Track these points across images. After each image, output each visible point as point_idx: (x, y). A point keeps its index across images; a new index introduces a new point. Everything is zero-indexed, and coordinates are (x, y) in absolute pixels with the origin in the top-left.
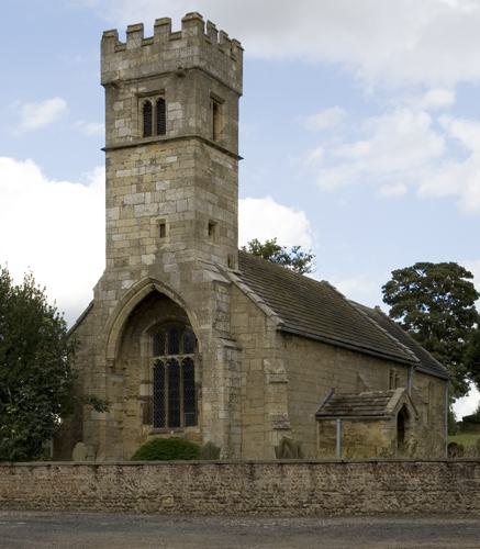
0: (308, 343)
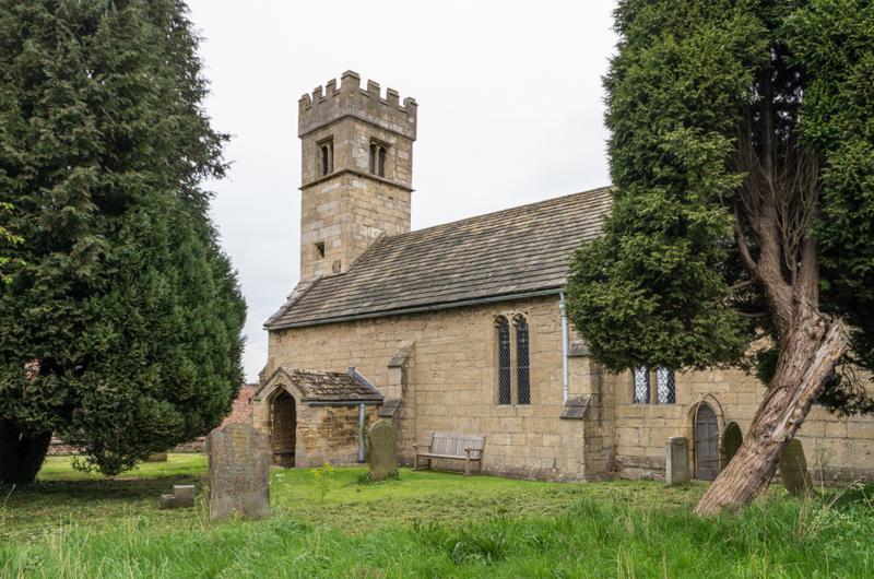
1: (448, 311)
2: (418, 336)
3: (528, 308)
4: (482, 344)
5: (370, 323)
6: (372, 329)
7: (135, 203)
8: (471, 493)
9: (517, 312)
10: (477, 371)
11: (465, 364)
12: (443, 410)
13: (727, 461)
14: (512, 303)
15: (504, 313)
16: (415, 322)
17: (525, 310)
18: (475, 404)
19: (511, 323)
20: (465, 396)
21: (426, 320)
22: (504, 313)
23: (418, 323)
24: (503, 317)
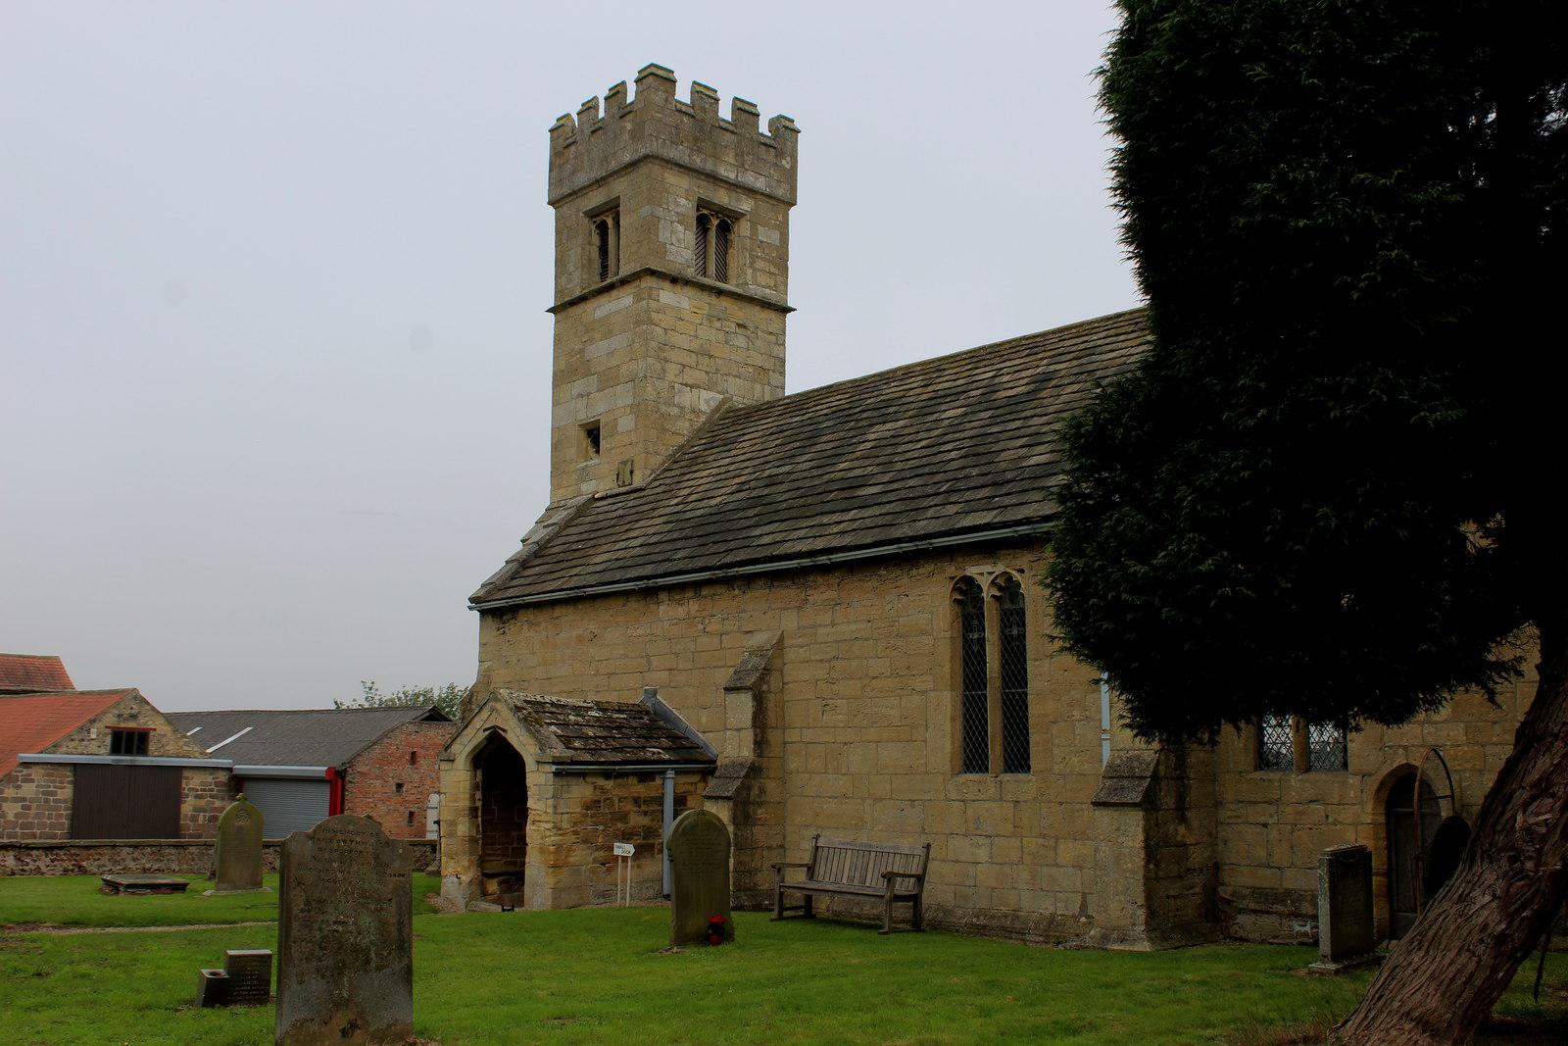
0: (558, 611)
2: (790, 622)
6: (694, 606)
9: (1000, 568)
10: (916, 699)
14: (988, 550)
16: (784, 592)
19: (988, 593)
22: (972, 571)
23: (788, 593)
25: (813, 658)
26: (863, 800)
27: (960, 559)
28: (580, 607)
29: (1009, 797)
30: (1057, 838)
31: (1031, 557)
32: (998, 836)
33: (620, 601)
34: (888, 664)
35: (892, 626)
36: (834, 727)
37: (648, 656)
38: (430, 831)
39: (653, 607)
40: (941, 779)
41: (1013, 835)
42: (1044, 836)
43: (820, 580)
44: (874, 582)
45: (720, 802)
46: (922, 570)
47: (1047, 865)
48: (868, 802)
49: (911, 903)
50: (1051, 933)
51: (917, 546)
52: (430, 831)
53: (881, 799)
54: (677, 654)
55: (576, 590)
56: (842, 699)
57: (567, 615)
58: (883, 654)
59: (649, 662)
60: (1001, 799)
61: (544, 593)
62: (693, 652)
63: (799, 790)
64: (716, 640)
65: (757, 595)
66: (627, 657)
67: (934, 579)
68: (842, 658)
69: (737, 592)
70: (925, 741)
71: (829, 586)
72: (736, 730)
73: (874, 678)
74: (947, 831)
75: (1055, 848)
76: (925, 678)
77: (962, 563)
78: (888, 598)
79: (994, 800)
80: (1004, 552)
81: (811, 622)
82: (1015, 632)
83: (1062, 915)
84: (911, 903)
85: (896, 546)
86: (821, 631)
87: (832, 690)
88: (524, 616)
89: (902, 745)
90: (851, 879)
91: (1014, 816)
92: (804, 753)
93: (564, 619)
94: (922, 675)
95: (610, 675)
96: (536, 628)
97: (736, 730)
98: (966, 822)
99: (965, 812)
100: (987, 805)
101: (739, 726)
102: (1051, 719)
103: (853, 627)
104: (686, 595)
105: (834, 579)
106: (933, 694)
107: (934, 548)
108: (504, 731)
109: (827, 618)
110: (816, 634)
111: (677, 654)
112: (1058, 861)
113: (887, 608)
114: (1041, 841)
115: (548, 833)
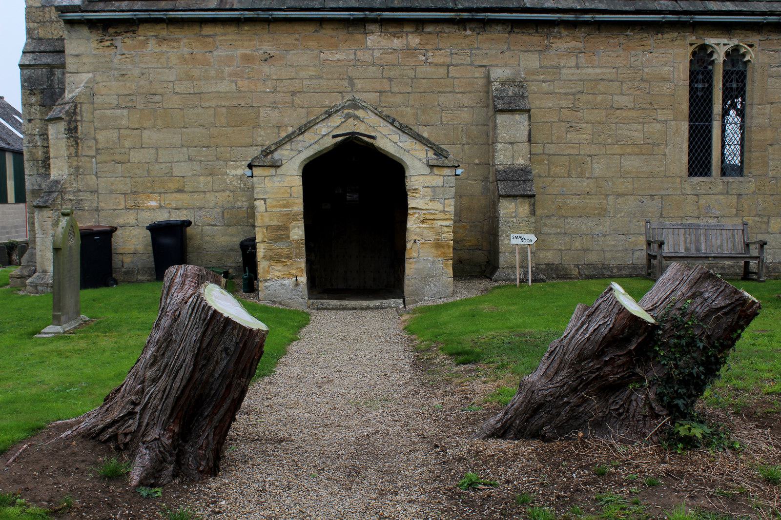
0: (208, 30)
1: (599, 26)
2: (531, 61)
3: (755, 39)
4: (667, 85)
5: (407, 29)
6: (414, 40)
7: (117, 434)
8: (97, 210)
9: (735, 42)
10: (658, 126)
11: (633, 114)
12: (585, 185)
13: (207, 176)
14: (727, 28)
15: (711, 41)
16: (526, 38)
17: (750, 40)
18: (651, 175)
19: (720, 57)
20: (631, 163)
21: (548, 36)
22: (711, 41)
23: (534, 39)
24: (703, 47)
25: (556, 91)
26: (607, 196)
27: (701, 32)
28: (246, 28)
29: (734, 191)
30: (769, 216)
31: (760, 37)
32: (724, 216)
33: (311, 28)
34: (632, 100)
35: (636, 73)
36: (579, 144)
37: (351, 79)
38: (258, 226)
39: (359, 36)
40: (678, 180)
41: (736, 216)
42: (759, 216)
43: (564, 32)
44: (622, 39)
45: (519, 200)
46: (666, 36)
47: (761, 233)
48: (611, 198)
49: (757, 262)
50: (772, 274)
51: (150, 15)
52: (258, 226)
53: (623, 195)
54: (390, 79)
55: (260, 12)
56: (588, 123)
57: (225, 38)
58: (628, 92)
59: (352, 84)
60: (727, 193)
61: (301, 10)
62: (412, 79)
63: (542, 190)
64: (442, 71)
65: (493, 37)
66: (321, 78)
67: (676, 43)
68: (586, 93)
69: (468, 32)
70: (665, 155)
71: (574, 38)
72: (510, 143)
73: (618, 109)
74: (682, 215)
75: (768, 223)
76: (665, 111)
77: (703, 34)
78: (633, 52)
79: (722, 194)
80: (738, 31)
81: (554, 63)
82: (734, 85)
83: (771, 263)
84: (757, 262)
85: (688, 16)
86: (564, 71)
87: (576, 116)
88: (144, 32)
89: (644, 157)
90: (686, 249)
91: (738, 204)
92: (546, 162)
93: (219, 38)
94: (663, 109)
95: (293, 93)
96: (175, 45)
97: (510, 143)
98: (698, 208)
99: (697, 202)
100: (717, 197)
101: (512, 140)
102: (769, 142)
103: (598, 71)
104: (405, 30)
105: (580, 33)
106: (673, 123)
107: (595, 21)
108: (374, 138)
109: (572, 62)
110: (560, 73)
111: (390, 79)
112: (770, 230)
113: (632, 60)
114: (757, 219)
115: (446, 229)
